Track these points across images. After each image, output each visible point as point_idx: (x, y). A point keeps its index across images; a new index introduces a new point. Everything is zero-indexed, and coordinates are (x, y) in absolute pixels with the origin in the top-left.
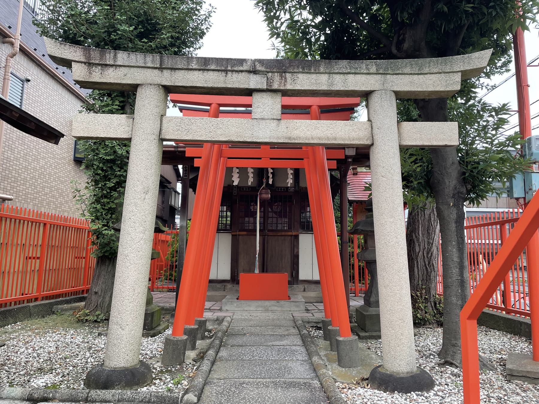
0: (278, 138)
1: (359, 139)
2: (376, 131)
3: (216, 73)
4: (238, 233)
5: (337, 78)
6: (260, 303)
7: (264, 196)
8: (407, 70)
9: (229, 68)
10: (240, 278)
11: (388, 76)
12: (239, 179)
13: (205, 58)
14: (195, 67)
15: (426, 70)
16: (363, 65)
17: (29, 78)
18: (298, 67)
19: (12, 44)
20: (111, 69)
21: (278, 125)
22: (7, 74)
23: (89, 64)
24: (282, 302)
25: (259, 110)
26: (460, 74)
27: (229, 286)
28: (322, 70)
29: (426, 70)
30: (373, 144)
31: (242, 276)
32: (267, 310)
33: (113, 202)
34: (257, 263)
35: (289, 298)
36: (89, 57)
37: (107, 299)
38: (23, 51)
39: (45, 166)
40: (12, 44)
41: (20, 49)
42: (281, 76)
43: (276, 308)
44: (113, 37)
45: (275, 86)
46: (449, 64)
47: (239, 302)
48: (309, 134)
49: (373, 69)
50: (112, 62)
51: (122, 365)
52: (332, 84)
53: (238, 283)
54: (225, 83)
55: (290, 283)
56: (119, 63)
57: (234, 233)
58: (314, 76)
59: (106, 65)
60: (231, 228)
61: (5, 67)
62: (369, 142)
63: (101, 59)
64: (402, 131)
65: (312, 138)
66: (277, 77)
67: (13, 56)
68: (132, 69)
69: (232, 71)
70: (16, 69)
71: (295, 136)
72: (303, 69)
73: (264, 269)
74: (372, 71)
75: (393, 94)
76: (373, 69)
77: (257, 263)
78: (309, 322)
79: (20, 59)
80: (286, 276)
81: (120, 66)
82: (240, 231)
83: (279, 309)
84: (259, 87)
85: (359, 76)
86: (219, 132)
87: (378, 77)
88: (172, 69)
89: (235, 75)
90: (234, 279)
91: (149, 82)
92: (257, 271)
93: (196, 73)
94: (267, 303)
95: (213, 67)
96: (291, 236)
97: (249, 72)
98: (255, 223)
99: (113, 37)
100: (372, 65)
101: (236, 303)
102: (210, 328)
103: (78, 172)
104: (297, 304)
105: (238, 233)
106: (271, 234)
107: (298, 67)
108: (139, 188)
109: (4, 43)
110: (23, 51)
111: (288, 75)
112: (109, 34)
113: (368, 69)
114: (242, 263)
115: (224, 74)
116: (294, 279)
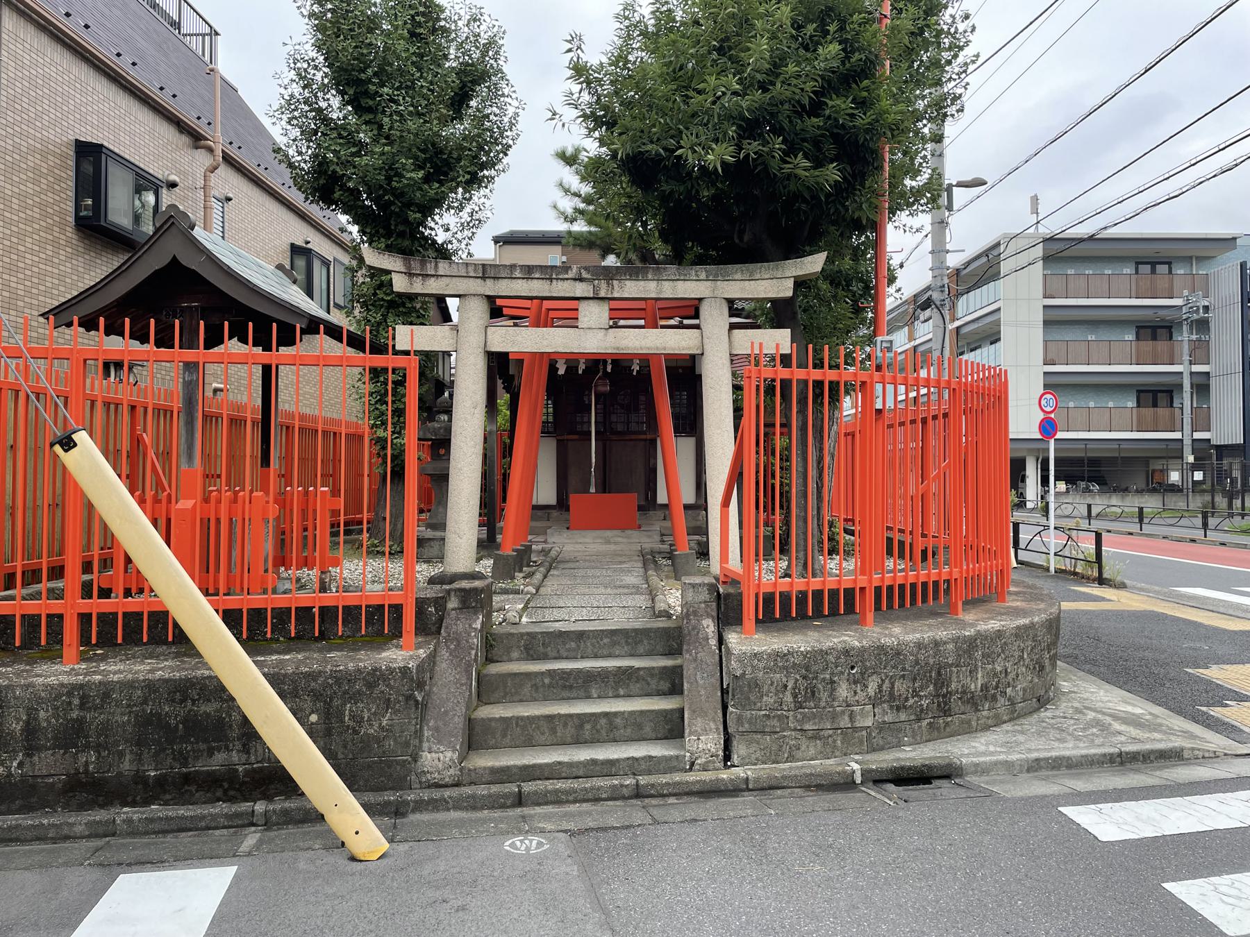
0: (606, 348)
1: (689, 348)
2: (706, 340)
3: (541, 282)
4: (566, 437)
5: (666, 284)
6: (598, 533)
7: (601, 389)
8: (738, 276)
9: (554, 276)
10: (571, 503)
11: (719, 283)
12: (565, 367)
13: (528, 266)
14: (518, 276)
15: (758, 276)
16: (692, 271)
17: (230, 195)
18: (625, 275)
19: (210, 150)
20: (433, 279)
21: (606, 335)
22: (208, 199)
23: (410, 275)
24: (629, 532)
25: (586, 319)
26: (793, 279)
27: (555, 513)
28: (650, 276)
29: (758, 276)
30: (703, 354)
31: (574, 499)
32: (608, 542)
33: (399, 400)
34: (593, 480)
35: (639, 527)
36: (409, 267)
37: (399, 526)
38: (227, 159)
39: (21, 248)
40: (210, 150)
41: (223, 157)
42: (608, 284)
43: (620, 539)
44: (394, 184)
45: (602, 294)
46: (781, 269)
47: (569, 533)
48: (637, 344)
49: (703, 276)
50: (433, 273)
51: (462, 570)
52: (661, 292)
53: (568, 509)
54: (550, 292)
55: (641, 508)
56: (441, 272)
57: (559, 438)
58: (642, 283)
59: (427, 275)
60: (555, 429)
61: (204, 188)
62: (699, 352)
63: (422, 269)
64: (733, 339)
65: (641, 348)
66: (603, 284)
67: (213, 169)
68: (454, 279)
69: (557, 279)
70: (18, 40)
71: (623, 346)
72: (631, 276)
73: (604, 487)
74: (701, 278)
75: (724, 301)
76: (703, 276)
77: (593, 480)
78: (660, 553)
79: (224, 172)
80: (634, 499)
81: (442, 276)
82: (569, 434)
83: (625, 540)
84: (586, 295)
85: (688, 283)
86: (545, 343)
87: (709, 283)
88: (494, 278)
89: (560, 283)
90: (562, 503)
91: (471, 292)
92: (593, 490)
93: (520, 281)
94: (608, 533)
95: (537, 276)
96: (646, 440)
97: (575, 279)
98: (590, 422)
99: (394, 184)
100: (702, 272)
101: (566, 534)
102: (535, 559)
103: (82, 250)
104: (649, 533)
105: (566, 437)
106: (614, 437)
107: (625, 275)
108: (468, 404)
109: (197, 148)
110: (227, 159)
111: (615, 282)
112: (389, 179)
113: (697, 275)
114: (573, 480)
115: (548, 282)
116: (649, 503)
